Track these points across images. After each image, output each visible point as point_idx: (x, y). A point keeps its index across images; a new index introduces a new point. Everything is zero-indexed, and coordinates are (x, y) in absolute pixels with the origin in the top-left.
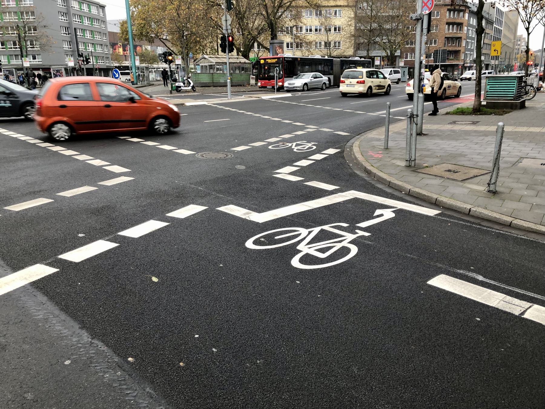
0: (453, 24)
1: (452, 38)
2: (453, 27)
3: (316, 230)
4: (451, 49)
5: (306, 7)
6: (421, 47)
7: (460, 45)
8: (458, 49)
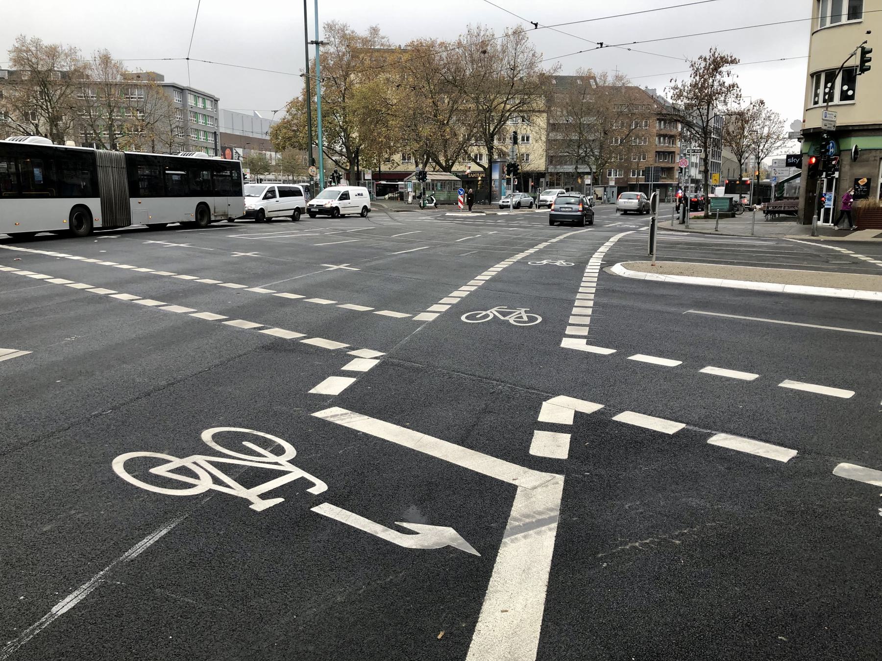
0: (665, 136)
1: (663, 152)
2: (664, 139)
3: (507, 318)
4: (663, 165)
5: (466, 152)
6: (206, 471)
7: (673, 161)
8: (671, 165)
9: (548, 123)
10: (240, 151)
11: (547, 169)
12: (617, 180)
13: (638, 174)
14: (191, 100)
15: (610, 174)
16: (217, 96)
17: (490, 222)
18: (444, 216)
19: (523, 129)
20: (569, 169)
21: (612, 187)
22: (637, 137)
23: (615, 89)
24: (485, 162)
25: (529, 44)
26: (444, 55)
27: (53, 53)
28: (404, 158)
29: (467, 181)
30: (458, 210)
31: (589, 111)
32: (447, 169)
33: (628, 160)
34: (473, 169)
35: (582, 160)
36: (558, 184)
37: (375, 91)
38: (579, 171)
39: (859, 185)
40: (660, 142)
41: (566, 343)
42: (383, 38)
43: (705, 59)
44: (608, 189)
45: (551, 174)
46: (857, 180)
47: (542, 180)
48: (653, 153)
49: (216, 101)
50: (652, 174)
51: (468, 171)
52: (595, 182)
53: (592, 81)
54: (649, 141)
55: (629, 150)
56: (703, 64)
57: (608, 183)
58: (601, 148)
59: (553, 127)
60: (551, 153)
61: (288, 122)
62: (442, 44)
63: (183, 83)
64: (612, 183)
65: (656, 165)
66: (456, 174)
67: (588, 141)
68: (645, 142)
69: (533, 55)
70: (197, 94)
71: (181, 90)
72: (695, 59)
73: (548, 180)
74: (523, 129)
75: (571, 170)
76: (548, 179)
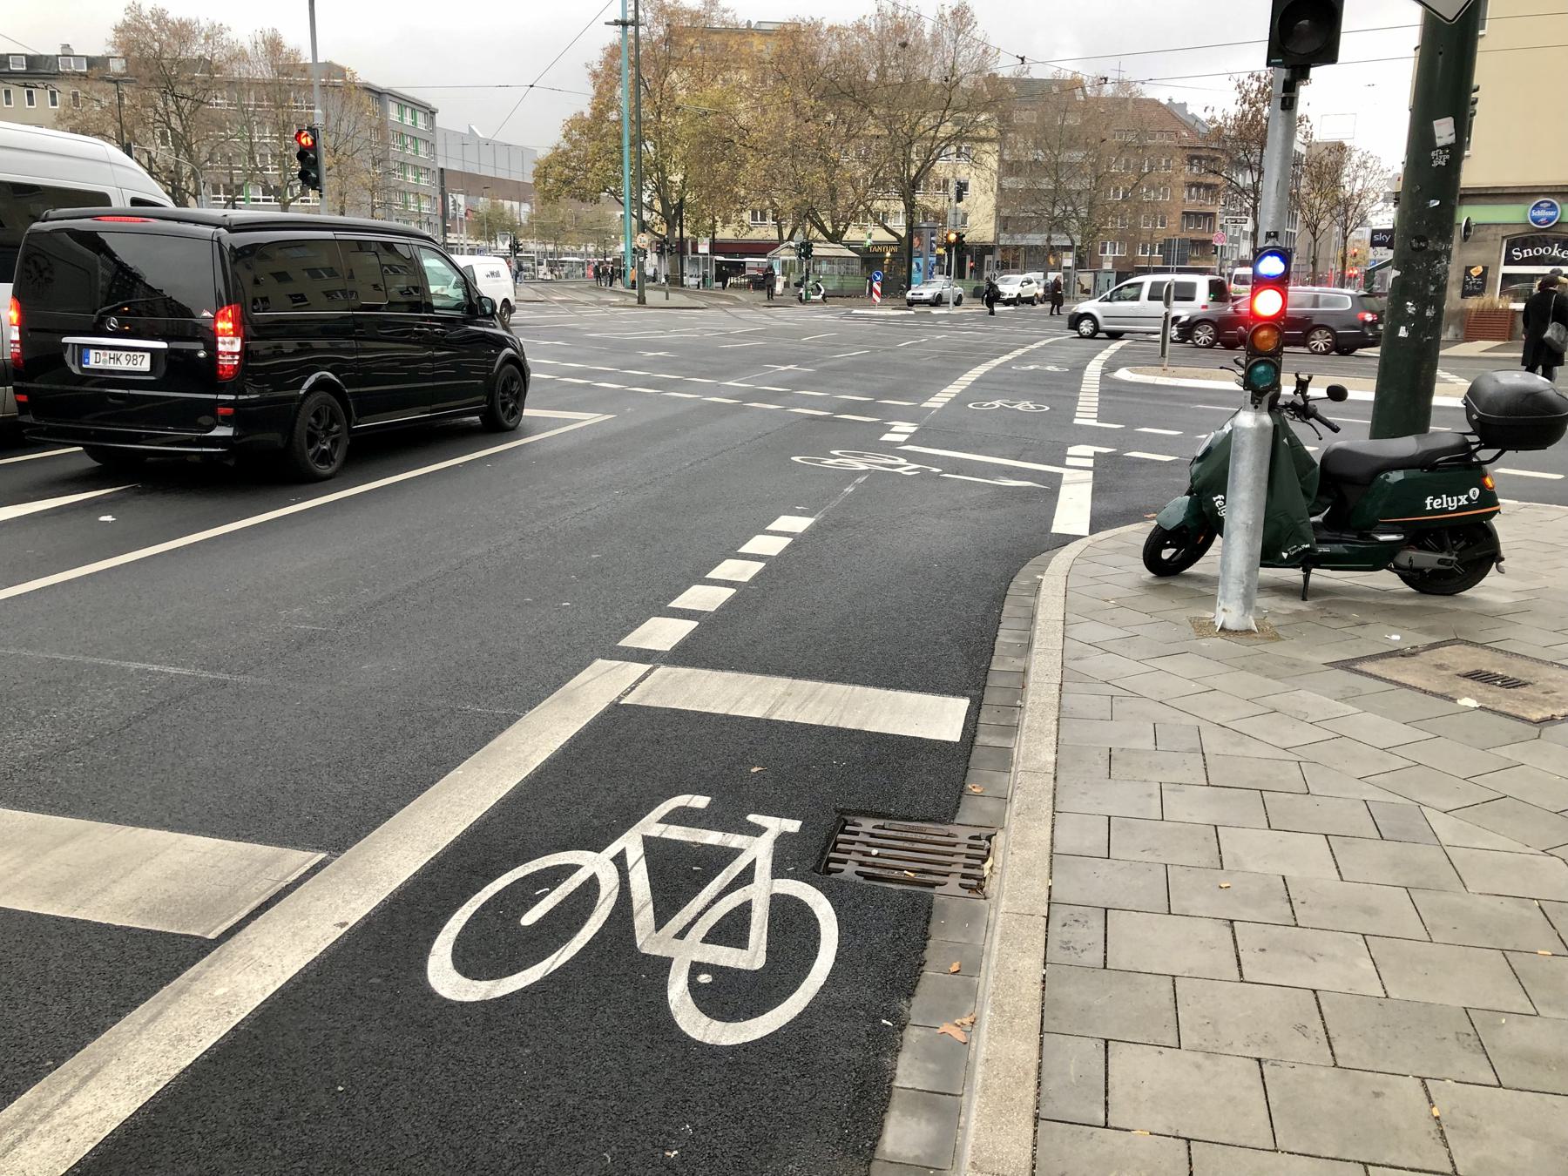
0: (1198, 186)
1: (1196, 214)
4: (1194, 236)
9: (1001, 161)
10: (461, 199)
11: (997, 238)
12: (1116, 261)
13: (1152, 251)
14: (393, 113)
15: (1104, 251)
16: (434, 105)
17: (927, 323)
18: (849, 313)
19: (964, 172)
20: (1037, 239)
21: (1107, 272)
22: (1151, 187)
23: (1118, 103)
24: (899, 225)
25: (978, 33)
26: (836, 47)
27: (183, 32)
28: (755, 219)
29: (870, 258)
30: (872, 305)
31: (1072, 142)
32: (835, 238)
33: (1134, 227)
34: (875, 238)
35: (1058, 225)
36: (1015, 266)
37: (721, 109)
38: (1054, 243)
39: (1470, 276)
40: (1190, 197)
41: (1076, 421)
42: (726, 11)
43: (1258, 79)
44: (1101, 276)
45: (1005, 249)
46: (1468, 269)
47: (988, 258)
48: (1178, 215)
49: (433, 113)
50: (1175, 254)
51: (869, 242)
52: (1080, 264)
53: (1079, 91)
54: (1172, 197)
55: (1137, 212)
56: (1256, 85)
57: (1100, 265)
58: (1091, 205)
59: (1010, 168)
60: (1005, 212)
61: (565, 153)
62: (831, 29)
63: (380, 83)
64: (1108, 266)
65: (1184, 235)
66: (848, 245)
67: (1069, 193)
68: (1165, 196)
69: (985, 52)
70: (404, 102)
71: (379, 95)
72: (1244, 77)
73: (998, 258)
74: (964, 172)
75: (1039, 243)
76: (998, 256)
